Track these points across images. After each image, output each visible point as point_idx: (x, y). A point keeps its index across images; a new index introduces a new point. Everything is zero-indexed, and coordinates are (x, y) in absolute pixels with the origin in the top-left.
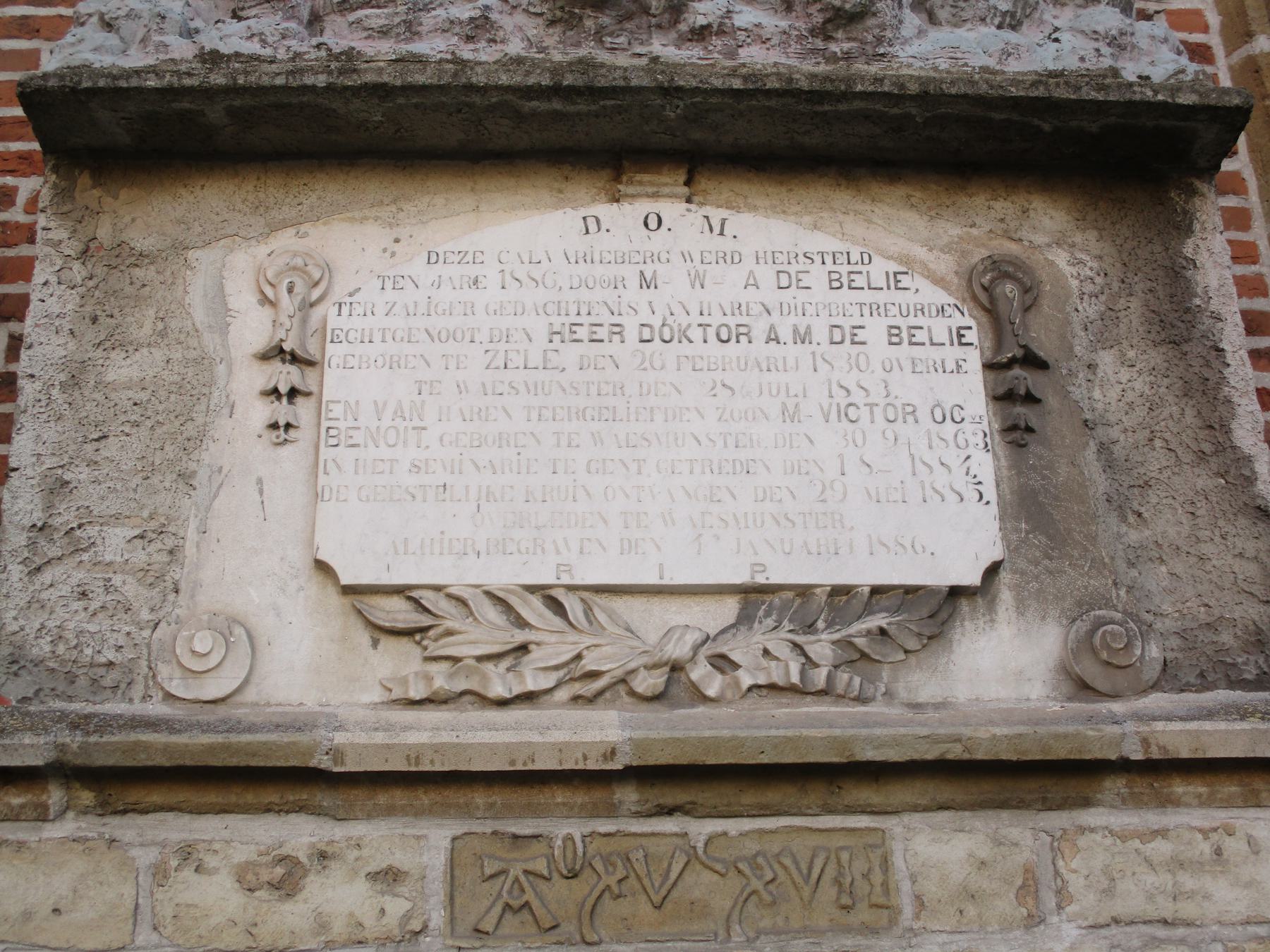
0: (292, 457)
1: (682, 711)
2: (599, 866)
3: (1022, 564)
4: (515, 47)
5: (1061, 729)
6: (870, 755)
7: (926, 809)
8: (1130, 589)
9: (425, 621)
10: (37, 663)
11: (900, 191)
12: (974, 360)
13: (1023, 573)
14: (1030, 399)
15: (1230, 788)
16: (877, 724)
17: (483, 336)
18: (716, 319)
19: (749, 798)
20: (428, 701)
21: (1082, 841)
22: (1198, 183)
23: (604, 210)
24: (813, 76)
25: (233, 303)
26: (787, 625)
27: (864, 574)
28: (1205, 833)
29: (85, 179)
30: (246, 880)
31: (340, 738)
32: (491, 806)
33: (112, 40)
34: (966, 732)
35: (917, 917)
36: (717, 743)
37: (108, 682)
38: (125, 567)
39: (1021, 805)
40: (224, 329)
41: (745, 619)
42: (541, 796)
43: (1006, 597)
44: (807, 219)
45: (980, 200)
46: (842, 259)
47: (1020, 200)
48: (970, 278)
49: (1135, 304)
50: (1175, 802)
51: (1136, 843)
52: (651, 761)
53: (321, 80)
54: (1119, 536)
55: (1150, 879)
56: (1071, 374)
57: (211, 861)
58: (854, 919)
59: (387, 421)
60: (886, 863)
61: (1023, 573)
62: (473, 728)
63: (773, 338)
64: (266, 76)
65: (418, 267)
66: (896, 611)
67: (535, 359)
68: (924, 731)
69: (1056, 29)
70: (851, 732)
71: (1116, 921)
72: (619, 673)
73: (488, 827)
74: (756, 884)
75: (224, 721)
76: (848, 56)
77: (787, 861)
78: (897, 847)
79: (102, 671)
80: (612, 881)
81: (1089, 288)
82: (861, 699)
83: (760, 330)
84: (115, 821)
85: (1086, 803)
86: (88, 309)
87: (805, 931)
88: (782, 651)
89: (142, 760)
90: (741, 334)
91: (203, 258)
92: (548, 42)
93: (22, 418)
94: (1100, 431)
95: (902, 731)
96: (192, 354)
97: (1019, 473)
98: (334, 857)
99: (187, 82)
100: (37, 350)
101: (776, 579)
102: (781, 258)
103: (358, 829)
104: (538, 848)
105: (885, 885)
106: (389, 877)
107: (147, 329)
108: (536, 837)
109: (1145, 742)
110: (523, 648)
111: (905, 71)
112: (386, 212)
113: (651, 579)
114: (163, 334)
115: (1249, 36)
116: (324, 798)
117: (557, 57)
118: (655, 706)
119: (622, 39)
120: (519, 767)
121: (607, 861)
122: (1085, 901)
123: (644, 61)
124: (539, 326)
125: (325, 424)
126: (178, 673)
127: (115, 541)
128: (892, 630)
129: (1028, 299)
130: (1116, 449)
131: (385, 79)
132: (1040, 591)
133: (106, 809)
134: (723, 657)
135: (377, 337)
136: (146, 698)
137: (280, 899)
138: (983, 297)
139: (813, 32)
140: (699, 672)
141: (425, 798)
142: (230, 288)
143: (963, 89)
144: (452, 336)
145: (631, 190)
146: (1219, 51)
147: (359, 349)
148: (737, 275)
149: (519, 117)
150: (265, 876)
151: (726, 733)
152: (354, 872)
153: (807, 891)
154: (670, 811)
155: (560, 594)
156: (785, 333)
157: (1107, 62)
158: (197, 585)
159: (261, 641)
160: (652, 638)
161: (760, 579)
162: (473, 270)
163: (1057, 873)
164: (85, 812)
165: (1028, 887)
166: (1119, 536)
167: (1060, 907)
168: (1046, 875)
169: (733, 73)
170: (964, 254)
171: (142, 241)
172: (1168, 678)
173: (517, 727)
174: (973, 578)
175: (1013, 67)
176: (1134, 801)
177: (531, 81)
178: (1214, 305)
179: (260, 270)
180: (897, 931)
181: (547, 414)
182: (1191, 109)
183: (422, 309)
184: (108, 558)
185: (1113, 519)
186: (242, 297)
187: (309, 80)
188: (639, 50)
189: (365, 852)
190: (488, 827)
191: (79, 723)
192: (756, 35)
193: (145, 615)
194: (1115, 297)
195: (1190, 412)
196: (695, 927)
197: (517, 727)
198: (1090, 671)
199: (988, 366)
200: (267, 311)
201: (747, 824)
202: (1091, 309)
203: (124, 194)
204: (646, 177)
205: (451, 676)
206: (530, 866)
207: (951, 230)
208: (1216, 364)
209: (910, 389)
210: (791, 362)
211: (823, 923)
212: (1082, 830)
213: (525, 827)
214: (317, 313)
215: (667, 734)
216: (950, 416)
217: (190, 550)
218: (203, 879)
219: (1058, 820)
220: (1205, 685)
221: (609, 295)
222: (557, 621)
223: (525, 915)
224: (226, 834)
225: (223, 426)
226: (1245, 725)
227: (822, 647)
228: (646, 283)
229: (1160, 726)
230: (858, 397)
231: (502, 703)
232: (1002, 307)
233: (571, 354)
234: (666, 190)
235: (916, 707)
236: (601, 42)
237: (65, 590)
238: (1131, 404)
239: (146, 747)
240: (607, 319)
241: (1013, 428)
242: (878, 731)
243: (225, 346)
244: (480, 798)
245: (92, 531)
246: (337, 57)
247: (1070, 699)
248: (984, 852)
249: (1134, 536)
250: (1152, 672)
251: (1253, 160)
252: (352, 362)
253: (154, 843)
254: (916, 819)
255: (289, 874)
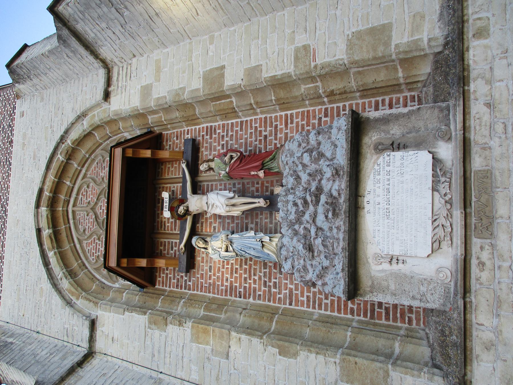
0: (408, 260)
1: (454, 201)
2: (480, 215)
3: (428, 147)
4: (342, 223)
5: (458, 144)
6: (462, 173)
7: (471, 164)
8: (432, 130)
9: (438, 240)
10: (444, 302)
11: (362, 163)
12: (392, 153)
13: (429, 147)
14: (399, 145)
15: (467, 117)
16: (457, 171)
17: (388, 230)
18: (385, 193)
19: (469, 192)
20: (451, 240)
21: (476, 140)
22: (360, 116)
23: (366, 210)
24: (347, 177)
25: (381, 269)
26: (439, 184)
27: (430, 172)
28: (475, 121)
29: (359, 292)
30: (482, 270)
31: (459, 254)
32: (470, 232)
33: (338, 286)
34: (458, 158)
35: (489, 166)
36: (460, 197)
37: (448, 291)
38: (427, 288)
39: (470, 149)
40: (386, 270)
41: (437, 191)
42: (468, 224)
43: (434, 150)
44: (367, 178)
45: (363, 151)
46: (375, 173)
47: (363, 144)
48: (377, 153)
49: (382, 127)
50: (470, 125)
51: (477, 131)
52: (463, 206)
53: (347, 253)
54: (423, 132)
55: (483, 130)
56: (394, 138)
57: (479, 276)
58: (489, 176)
59: (403, 245)
60: (480, 171)
61: (429, 147)
62: (457, 234)
63: (389, 184)
64: (346, 261)
65: (376, 239)
66: (436, 168)
67: (393, 222)
68: (458, 164)
69: (336, 138)
70: (458, 176)
71: (490, 135)
72: (447, 211)
73: (473, 232)
74: (483, 191)
75: (455, 272)
76: (343, 172)
77: (479, 186)
78: (477, 169)
79: (446, 292)
80: (483, 213)
81: (379, 134)
82: (452, 173)
83: (388, 187)
84: (472, 291)
85: (470, 139)
86: (382, 292)
87: (491, 184)
88: (443, 185)
89: (463, 285)
90: (388, 189)
91: (373, 273)
92: (341, 218)
93: (401, 303)
94: (404, 134)
95: (458, 168)
96: (390, 276)
97: (412, 147)
98: (478, 256)
99: (347, 274)
100: (389, 300)
101: (431, 186)
102: (375, 183)
103: (473, 252)
104: (477, 225)
105: (484, 171)
106: (482, 248)
107: (385, 283)
108: (475, 225)
109: (460, 130)
110: (443, 225)
111: (346, 163)
112: (365, 244)
113: (431, 205)
114: (387, 280)
115: (324, 102)
116: (468, 257)
117: (344, 216)
118: (452, 205)
119: (341, 207)
120: (464, 227)
121: (479, 214)
122: (487, 140)
123: (344, 203)
124: (387, 221)
125: (403, 255)
126: (446, 280)
127: (423, 289)
128: (440, 168)
129: (381, 144)
130: (408, 131)
131: (347, 243)
132: (433, 144)
133: (470, 292)
134: (444, 195)
135: (388, 246)
136: (450, 285)
137: (485, 265)
138: (381, 151)
139: (339, 177)
140: (447, 198)
141: (468, 242)
142: (378, 269)
143: (349, 154)
144: (388, 235)
145: (362, 206)
146: (326, 106)
147: (390, 249)
148: (377, 190)
149: (352, 223)
150: (481, 267)
151: (459, 195)
152: (481, 253)
153: (485, 183)
154: (471, 204)
155: (433, 219)
156: (388, 183)
157: (344, 132)
158: (431, 276)
159: (441, 266)
160: (441, 205)
161: (431, 188)
162: (377, 231)
163: (482, 144)
164: (470, 295)
165: (484, 149)
166: (423, 132)
167: (488, 144)
168: (482, 146)
169: (346, 190)
170: (373, 154)
171: (370, 283)
172: (448, 125)
173: (457, 227)
174: (431, 155)
175: (345, 146)
176: (469, 132)
177: (348, 221)
178: (382, 114)
179: (376, 264)
180: (492, 169)
181: (402, 220)
182: (352, 119)
183: (383, 239)
184: (426, 290)
185: (420, 132)
186: (380, 268)
187: (347, 255)
188: (342, 204)
189: (477, 251)
190: (473, 232)
191: (456, 295)
192: (340, 186)
193: (436, 284)
194: (380, 130)
195: (401, 119)
196: (491, 201)
197: (457, 227)
198: (447, 137)
199: (393, 151)
200: (383, 264)
201: (473, 192)
202: (383, 134)
203: (361, 286)
204: (360, 203)
205: (447, 237)
206: (480, 226)
207: (369, 155)
208: (393, 115)
209: (398, 163)
210: (393, 182)
211: (490, 181)
212: (474, 140)
213: (473, 227)
214: (383, 256)
215: (459, 204)
216: (403, 158)
217: (425, 277)
218: (482, 278)
219: (473, 144)
220: (449, 119)
221: (381, 210)
222: (438, 220)
223: (488, 227)
224: (474, 273)
225: (403, 271)
226: (458, 115)
227: (443, 179)
228: (379, 204)
229: (458, 128)
230: (399, 172)
231: (452, 229)
232: (383, 148)
233: (391, 216)
234: (362, 200)
235: (453, 165)
236: (341, 210)
237: (431, 297)
238: (400, 129)
239: (460, 284)
240: (385, 210)
241: (404, 147)
242: (458, 172)
243: (389, 270)
244: (468, 233)
245: (421, 292)
246: (343, 251)
247: (451, 141)
248: (478, 155)
249: (423, 129)
250: (447, 128)
251: (346, 102)
252: (393, 250)
253: (476, 285)
254: (472, 166)
255: (481, 264)
